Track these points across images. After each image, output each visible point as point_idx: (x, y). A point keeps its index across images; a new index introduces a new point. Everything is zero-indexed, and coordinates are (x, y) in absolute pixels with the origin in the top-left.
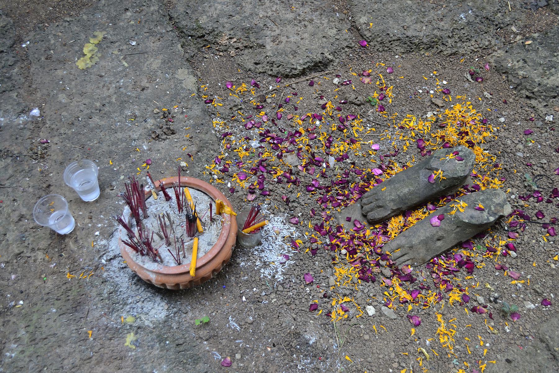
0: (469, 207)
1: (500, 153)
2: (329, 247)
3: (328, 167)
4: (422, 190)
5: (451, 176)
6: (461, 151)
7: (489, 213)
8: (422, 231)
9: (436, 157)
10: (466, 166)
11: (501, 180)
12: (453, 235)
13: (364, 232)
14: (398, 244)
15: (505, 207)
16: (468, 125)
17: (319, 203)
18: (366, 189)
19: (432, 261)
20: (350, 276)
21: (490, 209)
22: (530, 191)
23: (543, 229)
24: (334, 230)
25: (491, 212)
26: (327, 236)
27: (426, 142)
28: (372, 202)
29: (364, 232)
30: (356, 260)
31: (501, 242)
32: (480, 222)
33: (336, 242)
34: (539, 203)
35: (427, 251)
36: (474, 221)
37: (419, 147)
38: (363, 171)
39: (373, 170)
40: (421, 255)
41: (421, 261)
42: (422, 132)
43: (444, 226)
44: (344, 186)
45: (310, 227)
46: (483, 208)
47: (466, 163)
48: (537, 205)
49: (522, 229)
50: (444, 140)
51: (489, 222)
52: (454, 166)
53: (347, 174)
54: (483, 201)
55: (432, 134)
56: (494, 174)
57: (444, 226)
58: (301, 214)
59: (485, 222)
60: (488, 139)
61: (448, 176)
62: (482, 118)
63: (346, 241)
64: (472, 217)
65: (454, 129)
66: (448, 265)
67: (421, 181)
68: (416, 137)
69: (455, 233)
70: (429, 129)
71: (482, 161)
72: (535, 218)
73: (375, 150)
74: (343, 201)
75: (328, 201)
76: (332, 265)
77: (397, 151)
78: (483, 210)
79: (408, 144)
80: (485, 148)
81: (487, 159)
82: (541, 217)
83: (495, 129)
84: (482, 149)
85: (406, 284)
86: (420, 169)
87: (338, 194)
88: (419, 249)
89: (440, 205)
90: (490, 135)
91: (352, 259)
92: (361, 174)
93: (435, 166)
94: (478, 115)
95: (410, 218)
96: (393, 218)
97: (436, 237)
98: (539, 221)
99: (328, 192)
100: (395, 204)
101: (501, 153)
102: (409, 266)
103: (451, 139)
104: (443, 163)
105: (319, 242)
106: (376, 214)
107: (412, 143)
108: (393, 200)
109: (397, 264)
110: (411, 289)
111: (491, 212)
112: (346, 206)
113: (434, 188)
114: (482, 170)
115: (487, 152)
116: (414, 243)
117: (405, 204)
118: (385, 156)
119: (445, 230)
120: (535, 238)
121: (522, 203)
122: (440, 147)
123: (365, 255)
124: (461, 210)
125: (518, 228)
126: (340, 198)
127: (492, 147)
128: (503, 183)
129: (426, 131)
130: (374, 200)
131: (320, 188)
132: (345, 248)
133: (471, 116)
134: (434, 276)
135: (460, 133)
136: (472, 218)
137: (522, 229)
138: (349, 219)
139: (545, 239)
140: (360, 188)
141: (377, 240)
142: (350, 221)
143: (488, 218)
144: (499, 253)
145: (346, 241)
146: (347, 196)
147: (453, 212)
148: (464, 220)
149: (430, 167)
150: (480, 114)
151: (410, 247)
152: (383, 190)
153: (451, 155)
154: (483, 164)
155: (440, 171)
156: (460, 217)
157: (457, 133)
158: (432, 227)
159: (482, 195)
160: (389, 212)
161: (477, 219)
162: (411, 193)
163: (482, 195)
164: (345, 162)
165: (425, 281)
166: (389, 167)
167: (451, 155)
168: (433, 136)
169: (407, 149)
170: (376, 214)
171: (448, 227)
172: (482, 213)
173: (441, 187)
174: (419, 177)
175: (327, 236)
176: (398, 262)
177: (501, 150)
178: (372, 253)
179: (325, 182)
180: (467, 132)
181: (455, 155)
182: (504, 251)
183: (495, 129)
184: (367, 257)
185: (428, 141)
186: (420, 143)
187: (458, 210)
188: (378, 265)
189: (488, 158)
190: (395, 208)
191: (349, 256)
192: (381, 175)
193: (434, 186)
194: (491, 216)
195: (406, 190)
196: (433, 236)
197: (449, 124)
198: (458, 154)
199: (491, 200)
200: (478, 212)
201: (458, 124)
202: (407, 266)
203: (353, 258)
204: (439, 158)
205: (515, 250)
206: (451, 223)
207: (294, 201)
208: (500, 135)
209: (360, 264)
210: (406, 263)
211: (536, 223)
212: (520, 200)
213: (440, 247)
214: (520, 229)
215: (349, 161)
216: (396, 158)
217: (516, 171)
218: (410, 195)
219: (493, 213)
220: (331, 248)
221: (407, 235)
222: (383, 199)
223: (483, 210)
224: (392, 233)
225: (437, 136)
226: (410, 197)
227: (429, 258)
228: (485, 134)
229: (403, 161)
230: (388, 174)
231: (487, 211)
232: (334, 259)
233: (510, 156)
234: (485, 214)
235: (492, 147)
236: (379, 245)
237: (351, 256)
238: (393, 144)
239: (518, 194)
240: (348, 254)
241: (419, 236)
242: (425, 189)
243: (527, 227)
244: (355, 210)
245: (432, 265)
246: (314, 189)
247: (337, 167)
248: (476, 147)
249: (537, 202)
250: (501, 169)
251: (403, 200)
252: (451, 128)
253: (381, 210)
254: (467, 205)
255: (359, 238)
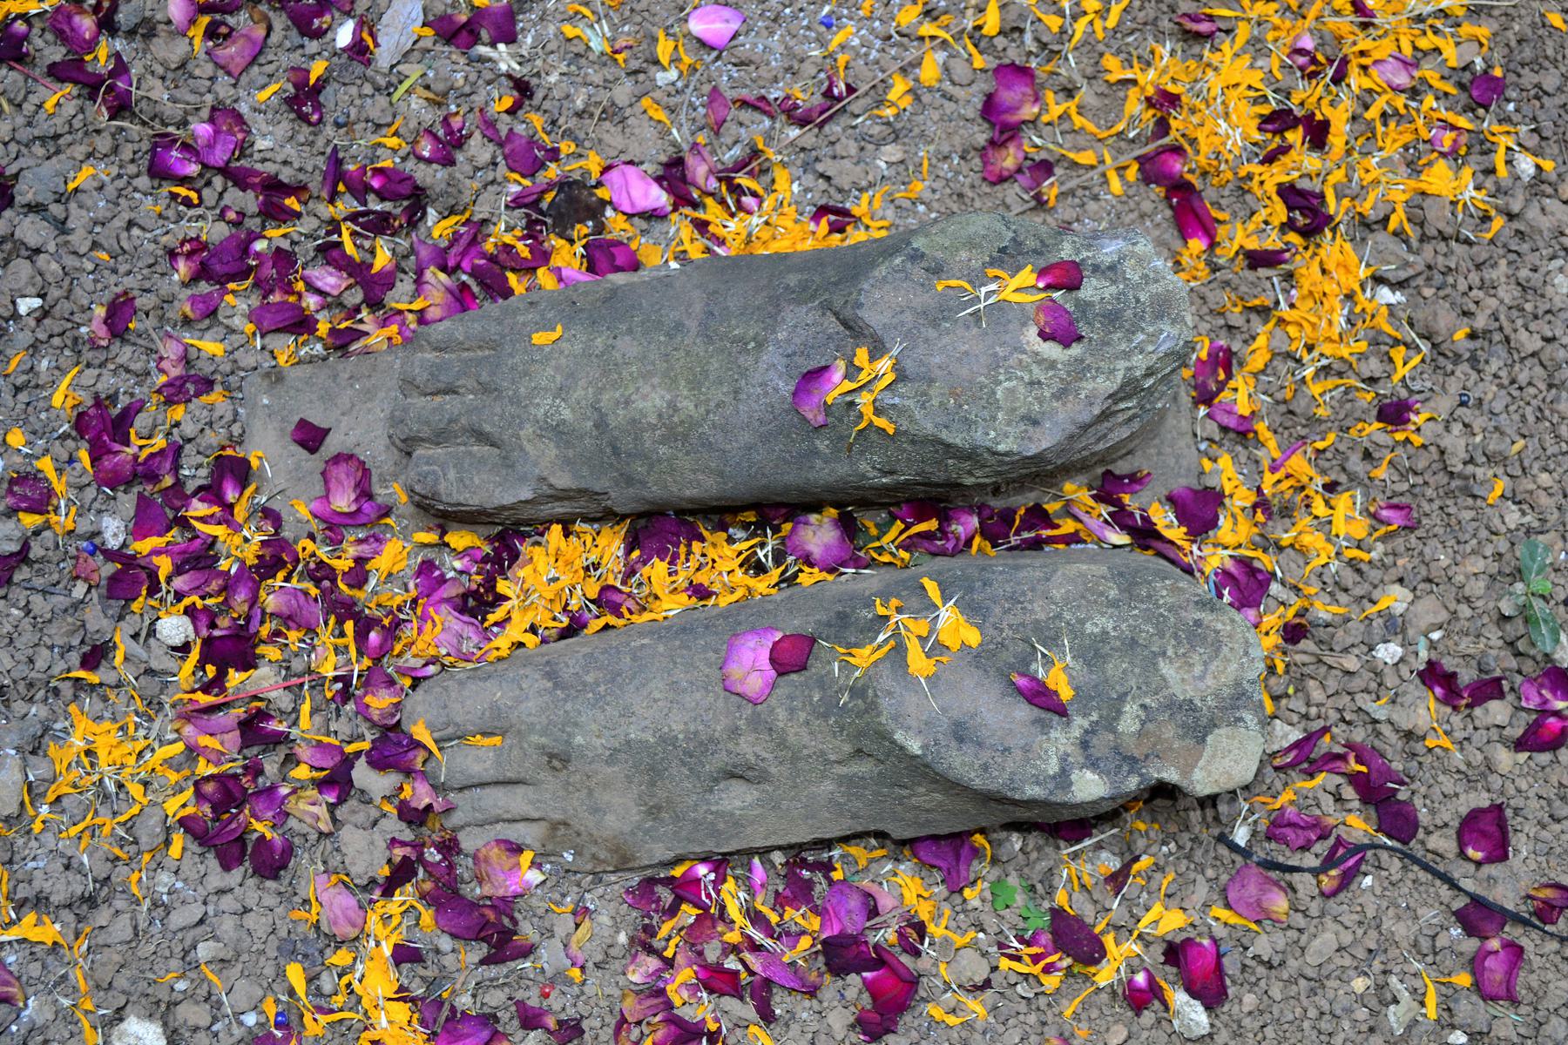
0: (977, 658)
1: (1460, 335)
2: (110, 569)
3: (359, 51)
4: (746, 437)
5: (929, 427)
6: (1111, 271)
7: (1084, 745)
8: (658, 688)
9: (917, 256)
10: (1060, 395)
11: (1374, 516)
12: (828, 786)
13: (365, 549)
14: (495, 709)
15: (1219, 738)
16: (1356, 80)
17: (183, 268)
18: (512, 278)
19: (678, 872)
20: (135, 790)
21: (1110, 722)
22: (1518, 654)
23: (1456, 932)
24: (195, 471)
25: (1102, 742)
26: (127, 502)
27: (1050, 96)
28: (451, 390)
29: (365, 549)
30: (226, 705)
31: (1157, 908)
32: (996, 782)
33: (156, 552)
34: (1523, 757)
35: (654, 812)
36: (961, 764)
37: (990, 108)
38: (554, 155)
39: (614, 175)
40: (610, 820)
41: (603, 855)
42: (1054, 22)
43: (782, 714)
44: (385, 217)
45: (57, 401)
46: (1066, 693)
47: (1080, 370)
48: (1505, 758)
49: (1328, 881)
50: (1163, 127)
51: (1059, 797)
52: (996, 363)
53: (449, 146)
54: (1092, 653)
55: (1111, 62)
56: (1356, 463)
57: (782, 714)
58: (37, 302)
59: (1032, 791)
60: (1438, 218)
61: (912, 420)
62: (1479, 65)
63: (223, 565)
64: (960, 733)
65: (1255, 78)
66: (758, 936)
67: (757, 378)
68: (1000, 42)
69: (842, 780)
70: (1112, 22)
71: (1327, 349)
72: (1444, 843)
73: (703, 44)
74: (331, 302)
75: (242, 275)
76: (67, 689)
77: (839, 99)
78: (1061, 711)
79: (929, 72)
80: (1388, 269)
81: (1363, 346)
82: (1479, 855)
83: (1526, 165)
84: (1363, 273)
85: (448, 961)
86: (802, 295)
87: (330, 253)
88: (606, 785)
89: (880, 550)
90: (1470, 192)
91: (206, 689)
92: (532, 168)
93: (873, 317)
94: (1467, 29)
95: (659, 567)
96: (557, 529)
97: (719, 760)
98: (1460, 871)
99: (274, 213)
100: (568, 462)
101: (1472, 336)
102: (527, 857)
103: (1201, 135)
104: (939, 315)
105: (63, 520)
106: (452, 475)
107: (960, 70)
108: (558, 432)
109: (456, 819)
110: (464, 1001)
111: (1102, 742)
112: (342, 341)
113: (815, 453)
114: (1300, 406)
115: (1386, 295)
116: (579, 740)
117: (629, 480)
118: (744, 104)
119: (782, 744)
120: (1377, 966)
121: (1425, 710)
122: (1123, 161)
123: (295, 690)
124: (918, 662)
125: (1310, 861)
126: (329, 279)
127: (1438, 278)
128: (1385, 539)
129: (1081, 26)
130: (471, 383)
131: (240, 179)
132: (190, 611)
133: (1420, 19)
134: (641, 970)
135: (1278, 121)
136: (961, 740)
137: (1328, 881)
138: (310, 437)
139: (1432, 1000)
140: (483, 255)
141: (409, 632)
142: (313, 450)
143: (1063, 778)
144: (1105, 975)
145: (223, 565)
146: (375, 288)
147: (864, 657)
148: (899, 736)
149: (848, 313)
150: (1483, 32)
151: (552, 756)
152: (539, 338)
153: (1027, 277)
154: (1325, 371)
155: (885, 364)
156: (884, 702)
157: (1265, 110)
158: (719, 689)
159: (1114, 604)
160: (526, 494)
161: (985, 755)
162: (676, 432)
163: (1114, 604)
164: (482, 59)
165: (571, 982)
166: (729, 182)
167: (1027, 277)
168: (1113, 78)
169: (906, 102)
170: (452, 475)
171: (804, 731)
172: (1045, 727)
173: (864, 466)
174: (760, 345)
175: (127, 502)
176: (465, 807)
177: (1481, 322)
178: (345, 695)
179: (289, 151)
180: (1325, 126)
181: (1048, 287)
182: (1140, 978)
183: (1526, 165)
184: (306, 708)
185: (1069, 92)
186: (1007, 97)
187: (899, 650)
188: (337, 781)
189: (1374, 344)
190: (563, 480)
191: (201, 665)
192: (654, 215)
193: (822, 445)
194: (1093, 764)
195: (651, 400)
196: (706, 745)
197: (1243, 32)
198: (1073, 286)
199: (1151, 664)
200: (1024, 712)
201: (1301, 52)
202: (516, 849)
203: (217, 684)
204: (937, 271)
205: (1211, 992)
206: (825, 716)
207: (35, 208)
208: (1533, 213)
209: (235, 736)
210: (515, 833)
211: (1437, 874)
212: (1415, 689)
213: (737, 823)
214: (1315, 872)
215: (504, 58)
216: (808, 137)
217: (1501, 486)
218: (664, 441)
219: (1116, 749)
220: (114, 579)
221: (566, 674)
222: (515, 400)
223: (1061, 711)
224: (515, 616)
225: (1134, 82)
226: (662, 450)
227: (661, 852)
228: (1440, 178)
229: (845, 173)
230: (702, 226)
231: (1079, 723)
232: (96, 656)
233: (1523, 378)
234: (1061, 740)
235: (1438, 278)
236: (410, 661)
237: (211, 670)
238: (838, 39)
239: (1432, 645)
240: (195, 655)
241: (627, 713)
242: (765, 438)
243: (1368, 881)
244: (369, 394)
245: (666, 896)
246: (193, 169)
247: (413, 71)
248: (1333, 248)
249: (1519, 745)
250: (1417, 440)
251: (616, 451)
252: (1246, 60)
253: (482, 461)
254: (973, 637)
255: (321, 573)
